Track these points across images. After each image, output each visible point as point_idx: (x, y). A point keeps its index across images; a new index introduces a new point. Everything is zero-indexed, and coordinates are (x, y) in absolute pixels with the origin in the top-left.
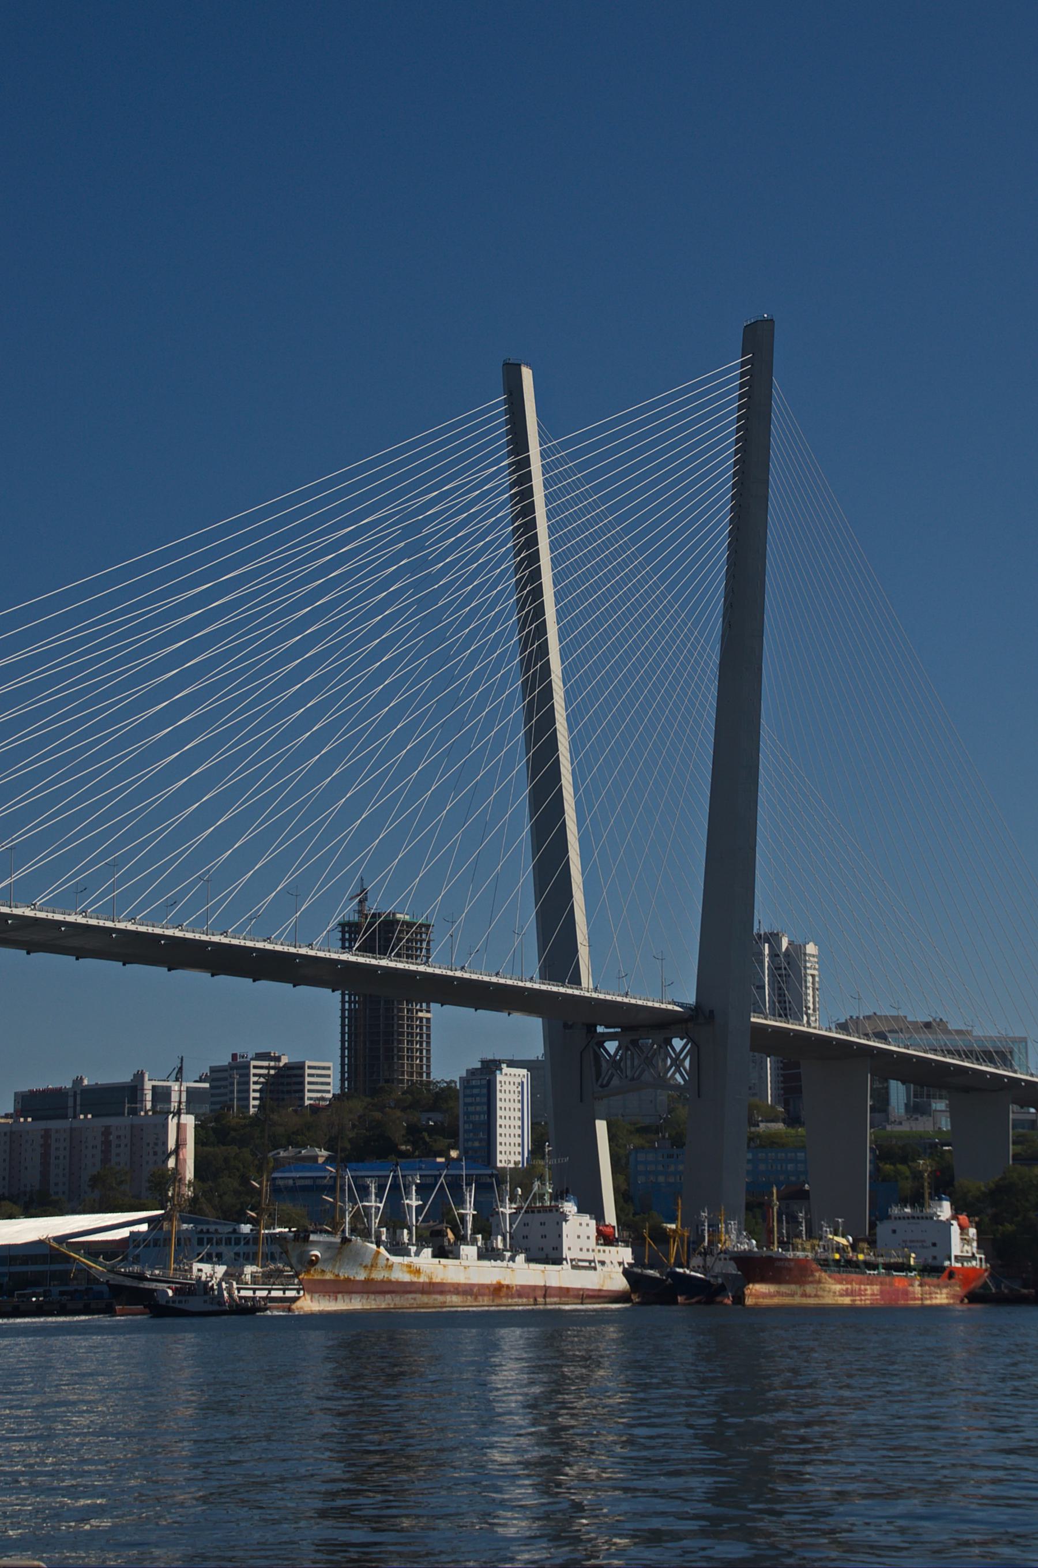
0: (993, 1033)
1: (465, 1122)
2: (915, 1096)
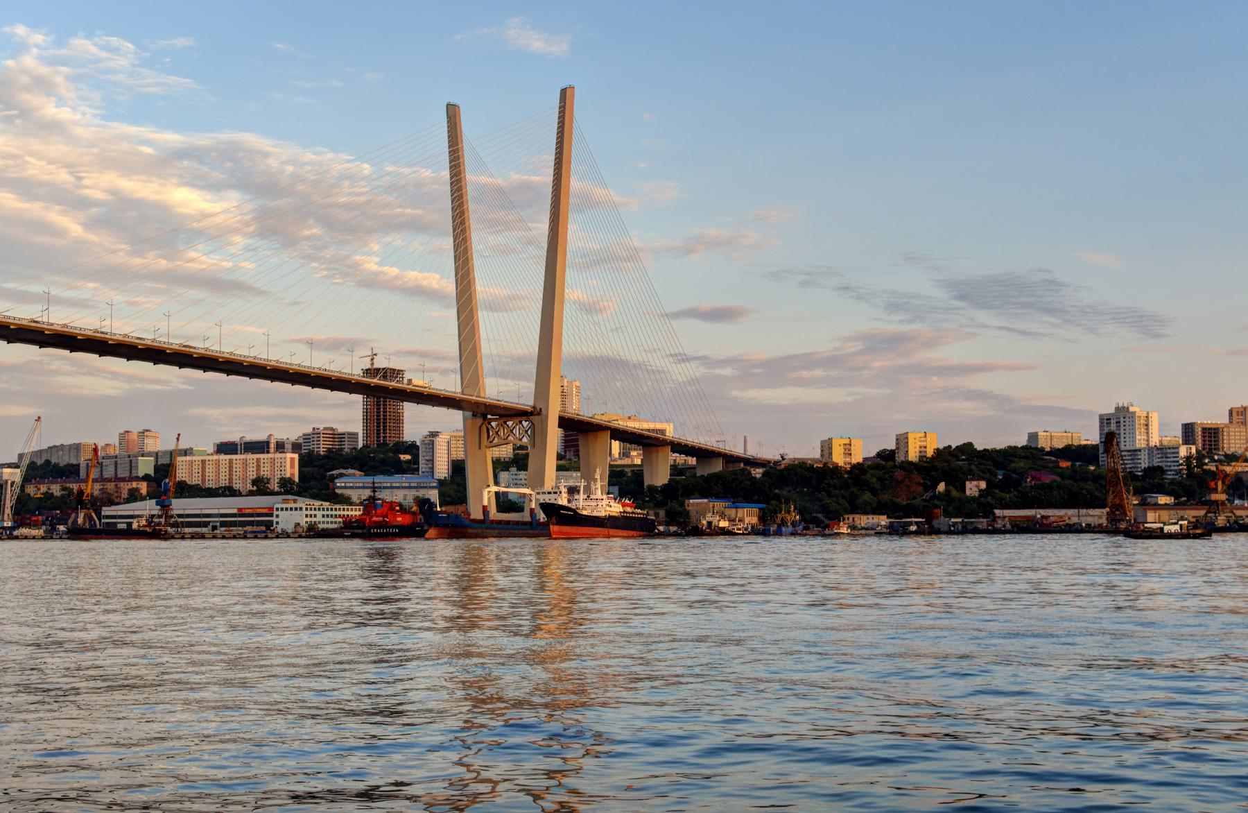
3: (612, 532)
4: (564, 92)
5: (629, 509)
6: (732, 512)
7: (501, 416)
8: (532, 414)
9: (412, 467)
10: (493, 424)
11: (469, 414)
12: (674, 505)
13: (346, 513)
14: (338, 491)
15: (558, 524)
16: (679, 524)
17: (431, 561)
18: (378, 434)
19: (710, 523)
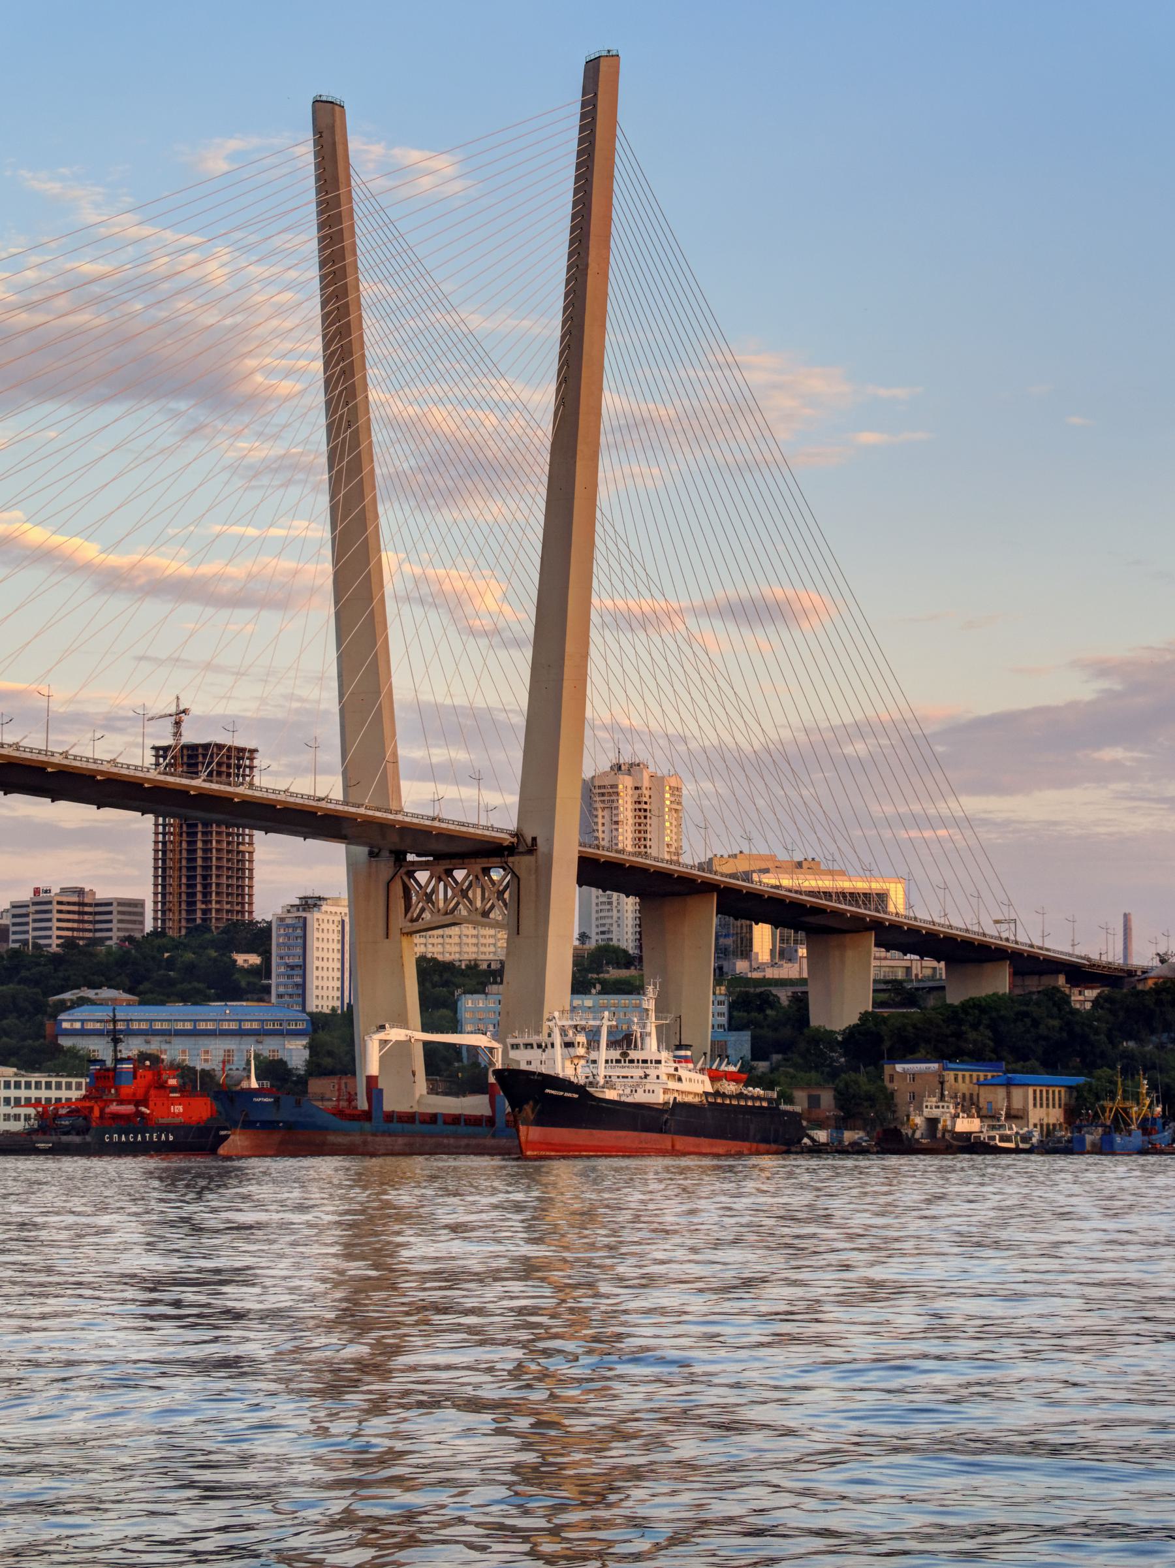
0: (368, 337)
1: (278, 965)
2: (782, 940)
3: (682, 1142)
4: (593, 67)
5: (730, 1088)
6: (997, 1098)
7: (439, 857)
8: (511, 850)
9: (254, 986)
10: (422, 876)
11: (362, 851)
12: (862, 1080)
13: (43, 1094)
14: (65, 1042)
15: (540, 1121)
16: (866, 1125)
17: (289, 1220)
18: (191, 903)
19: (932, 1122)
